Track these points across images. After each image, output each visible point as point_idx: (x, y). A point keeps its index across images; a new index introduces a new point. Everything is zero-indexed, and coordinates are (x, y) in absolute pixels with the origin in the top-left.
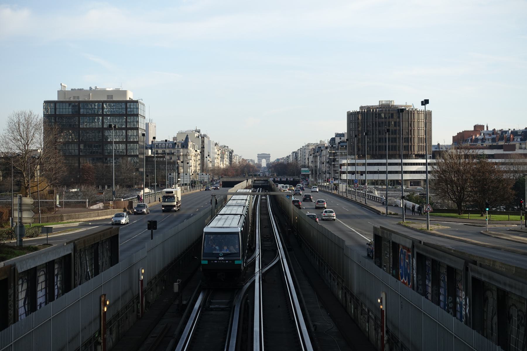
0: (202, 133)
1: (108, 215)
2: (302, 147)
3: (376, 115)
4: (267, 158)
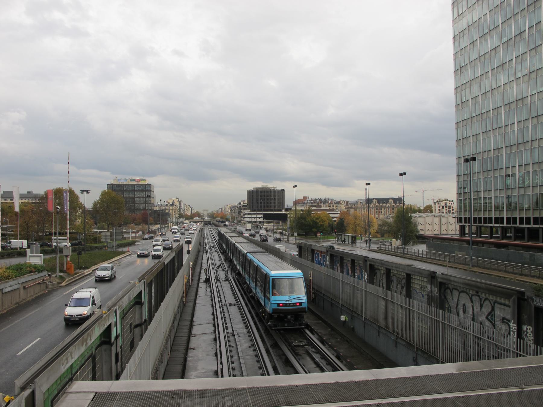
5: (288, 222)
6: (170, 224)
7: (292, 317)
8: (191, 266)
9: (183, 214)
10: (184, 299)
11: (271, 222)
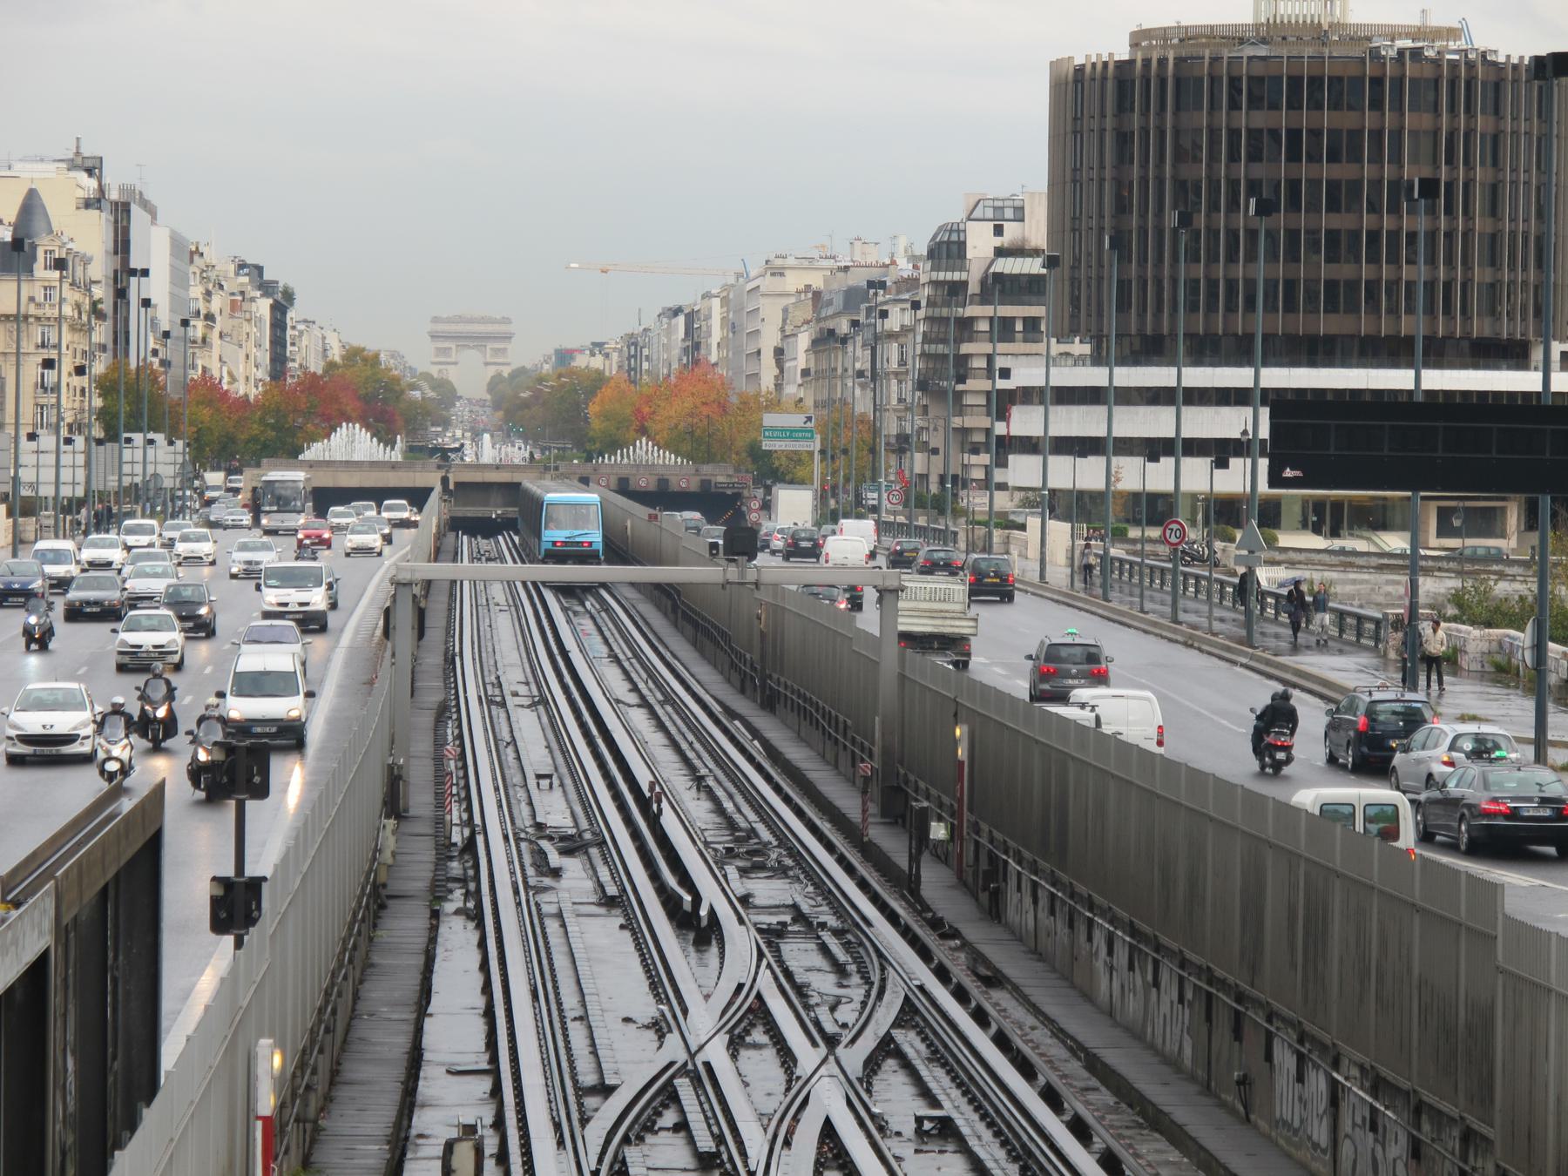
0: (115, 182)
3: (1234, 82)
4: (490, 345)
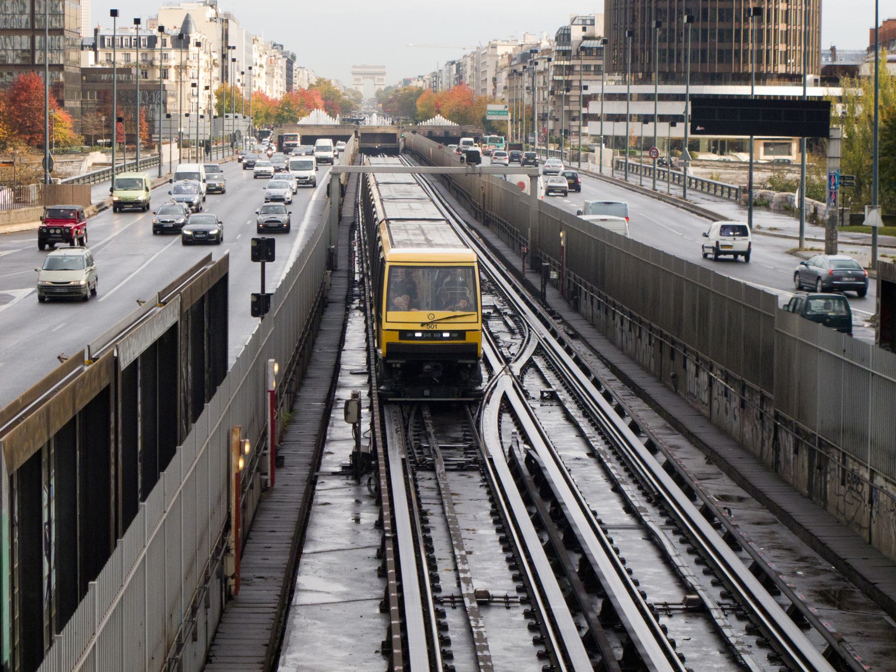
1: (13, 224)
2: (475, 50)
5: (835, 149)
6: (165, 148)
7: (436, 368)
8: (273, 385)
9: (244, 91)
10: (230, 567)
11: (738, 147)
